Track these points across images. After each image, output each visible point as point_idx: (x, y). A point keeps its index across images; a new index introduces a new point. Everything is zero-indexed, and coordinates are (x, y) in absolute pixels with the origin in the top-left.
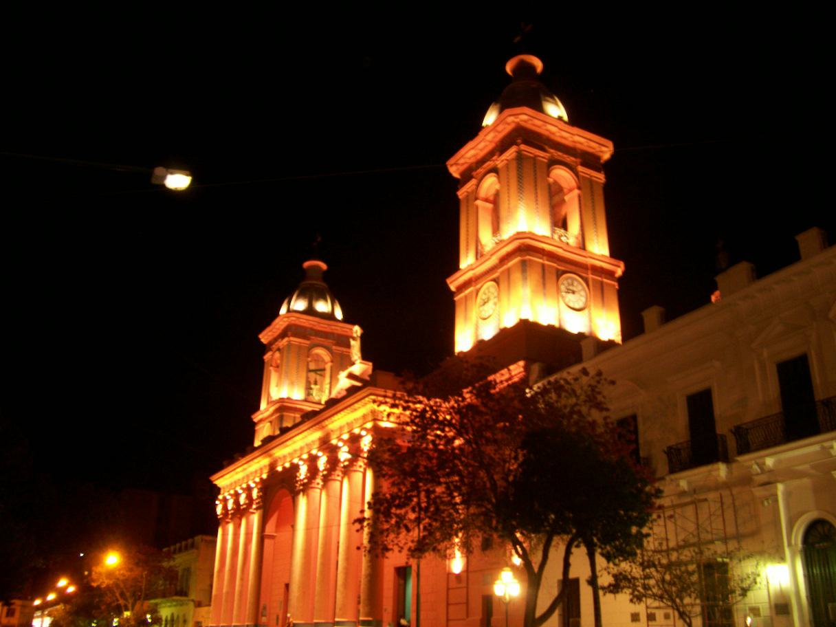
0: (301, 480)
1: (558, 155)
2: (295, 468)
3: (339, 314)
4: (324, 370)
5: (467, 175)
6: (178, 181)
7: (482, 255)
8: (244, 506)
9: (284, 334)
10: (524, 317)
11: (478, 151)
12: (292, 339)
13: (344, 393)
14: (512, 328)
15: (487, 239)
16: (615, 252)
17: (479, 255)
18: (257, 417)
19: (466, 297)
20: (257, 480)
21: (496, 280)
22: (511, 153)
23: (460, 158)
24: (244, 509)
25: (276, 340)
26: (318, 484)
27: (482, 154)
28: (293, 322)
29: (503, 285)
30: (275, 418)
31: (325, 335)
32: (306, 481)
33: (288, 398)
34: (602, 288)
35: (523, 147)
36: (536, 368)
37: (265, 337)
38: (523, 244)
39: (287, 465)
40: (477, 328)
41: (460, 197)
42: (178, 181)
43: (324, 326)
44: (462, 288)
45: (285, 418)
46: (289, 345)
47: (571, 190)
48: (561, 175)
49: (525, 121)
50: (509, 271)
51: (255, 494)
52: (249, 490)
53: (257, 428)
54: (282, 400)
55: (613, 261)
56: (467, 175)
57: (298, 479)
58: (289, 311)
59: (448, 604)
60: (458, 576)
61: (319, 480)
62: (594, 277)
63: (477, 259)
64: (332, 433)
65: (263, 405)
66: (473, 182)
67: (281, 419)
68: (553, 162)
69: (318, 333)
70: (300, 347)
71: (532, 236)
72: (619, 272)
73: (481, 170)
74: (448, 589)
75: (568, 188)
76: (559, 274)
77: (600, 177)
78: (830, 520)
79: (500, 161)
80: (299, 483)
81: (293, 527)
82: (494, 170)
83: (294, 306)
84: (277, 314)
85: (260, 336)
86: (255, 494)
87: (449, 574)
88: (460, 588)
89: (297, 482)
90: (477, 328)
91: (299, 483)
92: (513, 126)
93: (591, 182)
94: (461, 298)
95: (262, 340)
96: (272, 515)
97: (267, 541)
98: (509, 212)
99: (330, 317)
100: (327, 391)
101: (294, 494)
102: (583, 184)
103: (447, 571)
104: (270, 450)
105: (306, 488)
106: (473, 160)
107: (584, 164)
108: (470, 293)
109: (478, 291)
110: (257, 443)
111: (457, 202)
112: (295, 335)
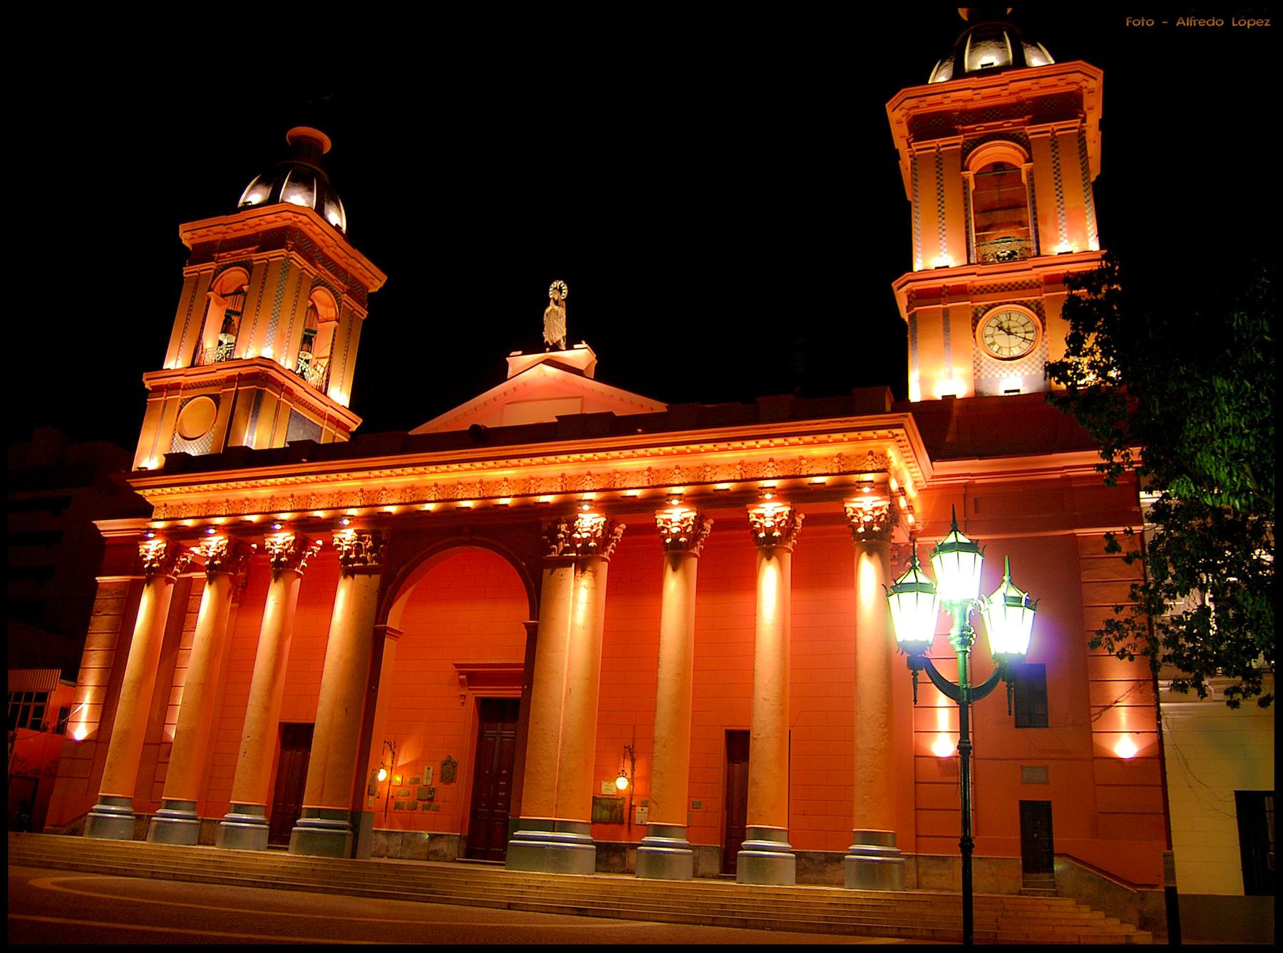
1: (327, 274)
5: (204, 252)
6: (1009, 10)
12: (294, 254)
15: (211, 343)
16: (354, 406)
28: (300, 225)
38: (264, 371)
42: (1009, 10)
45: (266, 396)
55: (349, 414)
56: (204, 252)
62: (328, 429)
66: (212, 265)
68: (319, 283)
72: (354, 428)
73: (227, 257)
75: (325, 317)
78: (1014, 164)
82: (247, 266)
83: (971, 64)
85: (182, 228)
93: (352, 316)
102: (344, 316)
107: (350, 293)
111: (179, 281)
112: (300, 251)
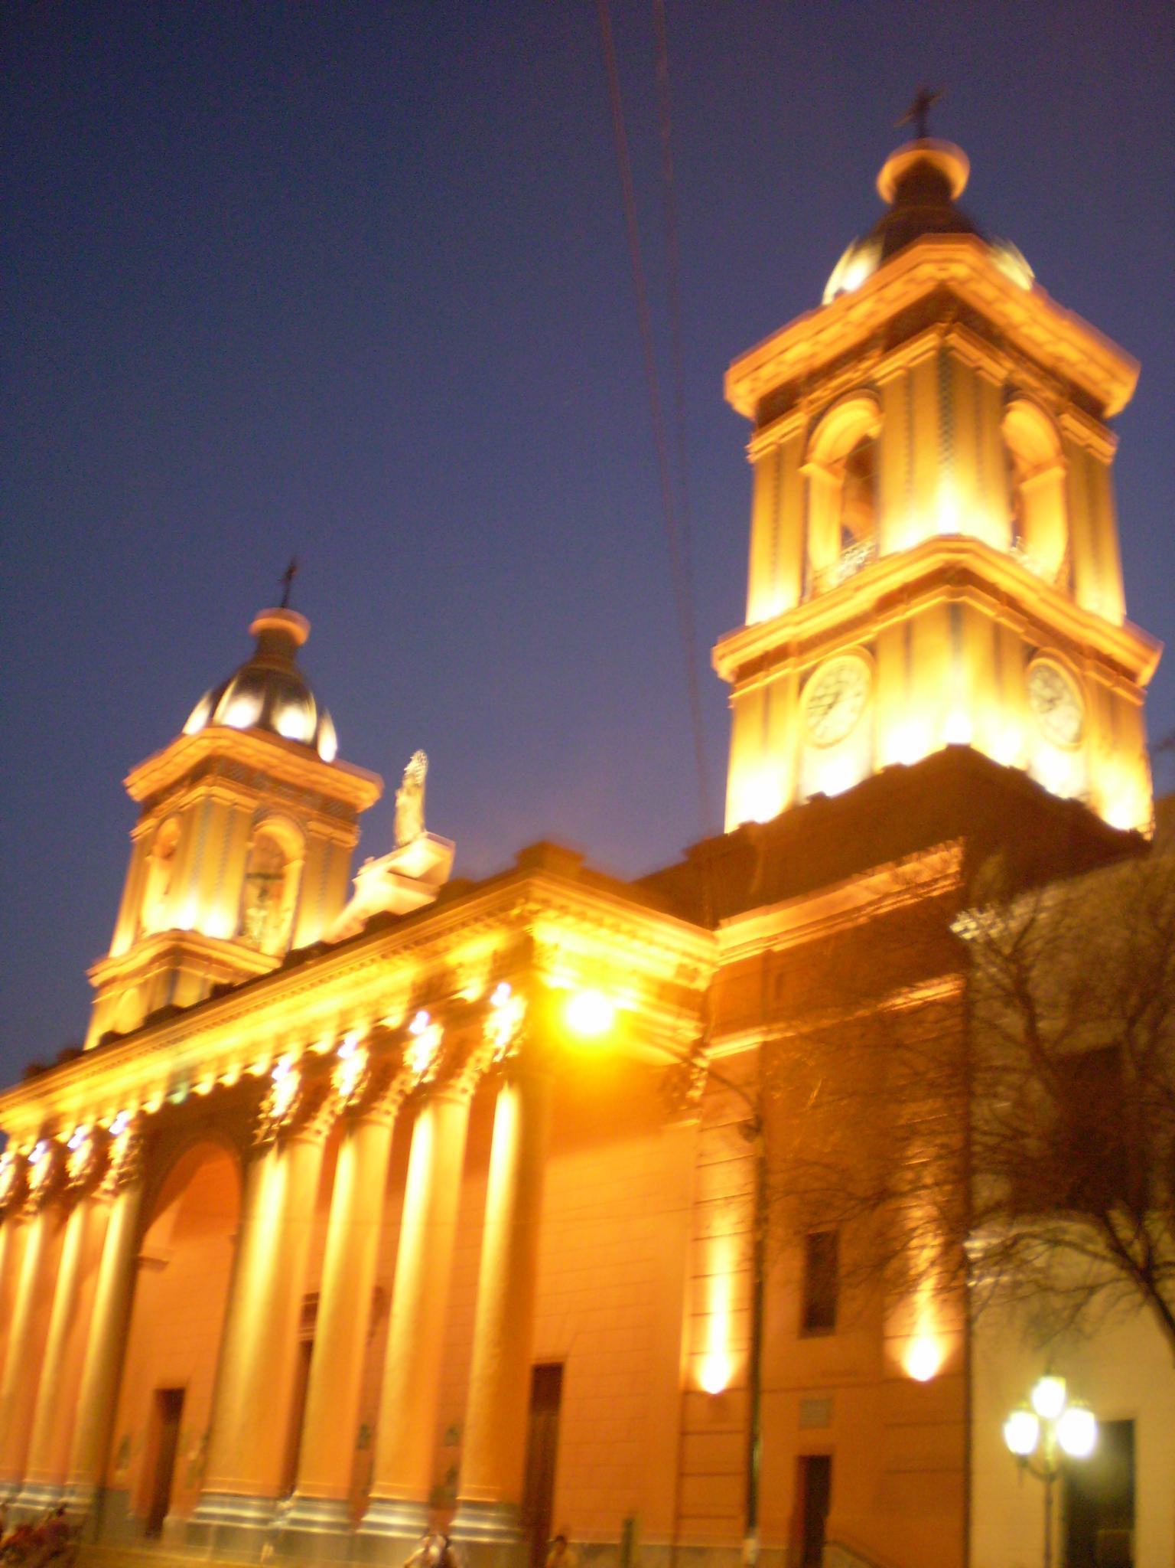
0: (274, 1121)
1: (1024, 377)
2: (254, 1088)
3: (328, 747)
4: (280, 876)
5: (151, 803)
7: (815, 595)
8: (80, 1182)
9: (197, 774)
10: (960, 739)
11: (818, 348)
13: (358, 929)
14: (827, 797)
17: (808, 589)
18: (101, 974)
19: (767, 692)
20: (130, 1114)
21: (872, 650)
22: (921, 349)
23: (177, 754)
24: (75, 1189)
25: (170, 789)
26: (319, 1132)
27: (827, 355)
28: (221, 751)
29: (890, 661)
30: (157, 976)
31: (299, 792)
32: (286, 1122)
33: (193, 932)
34: (1110, 705)
35: (954, 339)
36: (991, 869)
37: (140, 784)
39: (230, 1080)
40: (799, 765)
41: (753, 458)
43: (294, 768)
44: (747, 670)
46: (209, 803)
47: (1039, 468)
48: (283, 832)
49: (228, 748)
50: (908, 630)
51: (118, 1150)
52: (102, 1138)
53: (101, 999)
54: (178, 935)
56: (151, 803)
57: (262, 1116)
58: (210, 722)
59: (681, 1475)
60: (718, 1401)
61: (322, 1123)
63: (801, 603)
64: (460, 971)
65: (122, 942)
67: (172, 979)
69: (279, 785)
70: (232, 814)
71: (975, 547)
74: (683, 1433)
76: (1031, 653)
77: (1105, 449)
79: (888, 368)
80: (265, 1127)
81: (239, 1240)
82: (870, 389)
83: (224, 714)
84: (174, 731)
86: (118, 1150)
87: (689, 1393)
88: (721, 1433)
89: (259, 1124)
90: (799, 765)
91: (265, 1127)
92: (927, 288)
94: (753, 694)
95: (132, 791)
96: (162, 1208)
97: (146, 1276)
98: (909, 481)
99: (309, 749)
100: (286, 926)
101: (249, 1156)
103: (682, 1385)
104: (439, 935)
105: (288, 1136)
106: (799, 369)
108: (785, 680)
109: (804, 679)
110: (92, 1043)
